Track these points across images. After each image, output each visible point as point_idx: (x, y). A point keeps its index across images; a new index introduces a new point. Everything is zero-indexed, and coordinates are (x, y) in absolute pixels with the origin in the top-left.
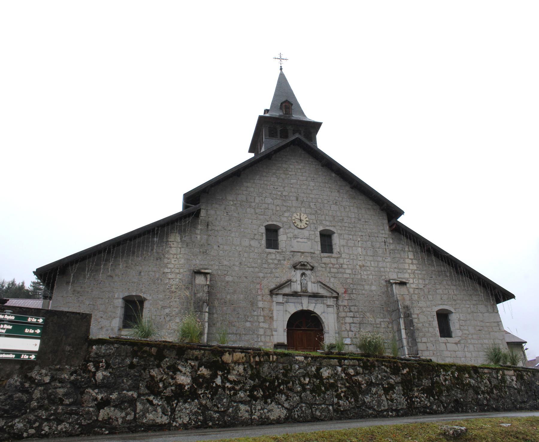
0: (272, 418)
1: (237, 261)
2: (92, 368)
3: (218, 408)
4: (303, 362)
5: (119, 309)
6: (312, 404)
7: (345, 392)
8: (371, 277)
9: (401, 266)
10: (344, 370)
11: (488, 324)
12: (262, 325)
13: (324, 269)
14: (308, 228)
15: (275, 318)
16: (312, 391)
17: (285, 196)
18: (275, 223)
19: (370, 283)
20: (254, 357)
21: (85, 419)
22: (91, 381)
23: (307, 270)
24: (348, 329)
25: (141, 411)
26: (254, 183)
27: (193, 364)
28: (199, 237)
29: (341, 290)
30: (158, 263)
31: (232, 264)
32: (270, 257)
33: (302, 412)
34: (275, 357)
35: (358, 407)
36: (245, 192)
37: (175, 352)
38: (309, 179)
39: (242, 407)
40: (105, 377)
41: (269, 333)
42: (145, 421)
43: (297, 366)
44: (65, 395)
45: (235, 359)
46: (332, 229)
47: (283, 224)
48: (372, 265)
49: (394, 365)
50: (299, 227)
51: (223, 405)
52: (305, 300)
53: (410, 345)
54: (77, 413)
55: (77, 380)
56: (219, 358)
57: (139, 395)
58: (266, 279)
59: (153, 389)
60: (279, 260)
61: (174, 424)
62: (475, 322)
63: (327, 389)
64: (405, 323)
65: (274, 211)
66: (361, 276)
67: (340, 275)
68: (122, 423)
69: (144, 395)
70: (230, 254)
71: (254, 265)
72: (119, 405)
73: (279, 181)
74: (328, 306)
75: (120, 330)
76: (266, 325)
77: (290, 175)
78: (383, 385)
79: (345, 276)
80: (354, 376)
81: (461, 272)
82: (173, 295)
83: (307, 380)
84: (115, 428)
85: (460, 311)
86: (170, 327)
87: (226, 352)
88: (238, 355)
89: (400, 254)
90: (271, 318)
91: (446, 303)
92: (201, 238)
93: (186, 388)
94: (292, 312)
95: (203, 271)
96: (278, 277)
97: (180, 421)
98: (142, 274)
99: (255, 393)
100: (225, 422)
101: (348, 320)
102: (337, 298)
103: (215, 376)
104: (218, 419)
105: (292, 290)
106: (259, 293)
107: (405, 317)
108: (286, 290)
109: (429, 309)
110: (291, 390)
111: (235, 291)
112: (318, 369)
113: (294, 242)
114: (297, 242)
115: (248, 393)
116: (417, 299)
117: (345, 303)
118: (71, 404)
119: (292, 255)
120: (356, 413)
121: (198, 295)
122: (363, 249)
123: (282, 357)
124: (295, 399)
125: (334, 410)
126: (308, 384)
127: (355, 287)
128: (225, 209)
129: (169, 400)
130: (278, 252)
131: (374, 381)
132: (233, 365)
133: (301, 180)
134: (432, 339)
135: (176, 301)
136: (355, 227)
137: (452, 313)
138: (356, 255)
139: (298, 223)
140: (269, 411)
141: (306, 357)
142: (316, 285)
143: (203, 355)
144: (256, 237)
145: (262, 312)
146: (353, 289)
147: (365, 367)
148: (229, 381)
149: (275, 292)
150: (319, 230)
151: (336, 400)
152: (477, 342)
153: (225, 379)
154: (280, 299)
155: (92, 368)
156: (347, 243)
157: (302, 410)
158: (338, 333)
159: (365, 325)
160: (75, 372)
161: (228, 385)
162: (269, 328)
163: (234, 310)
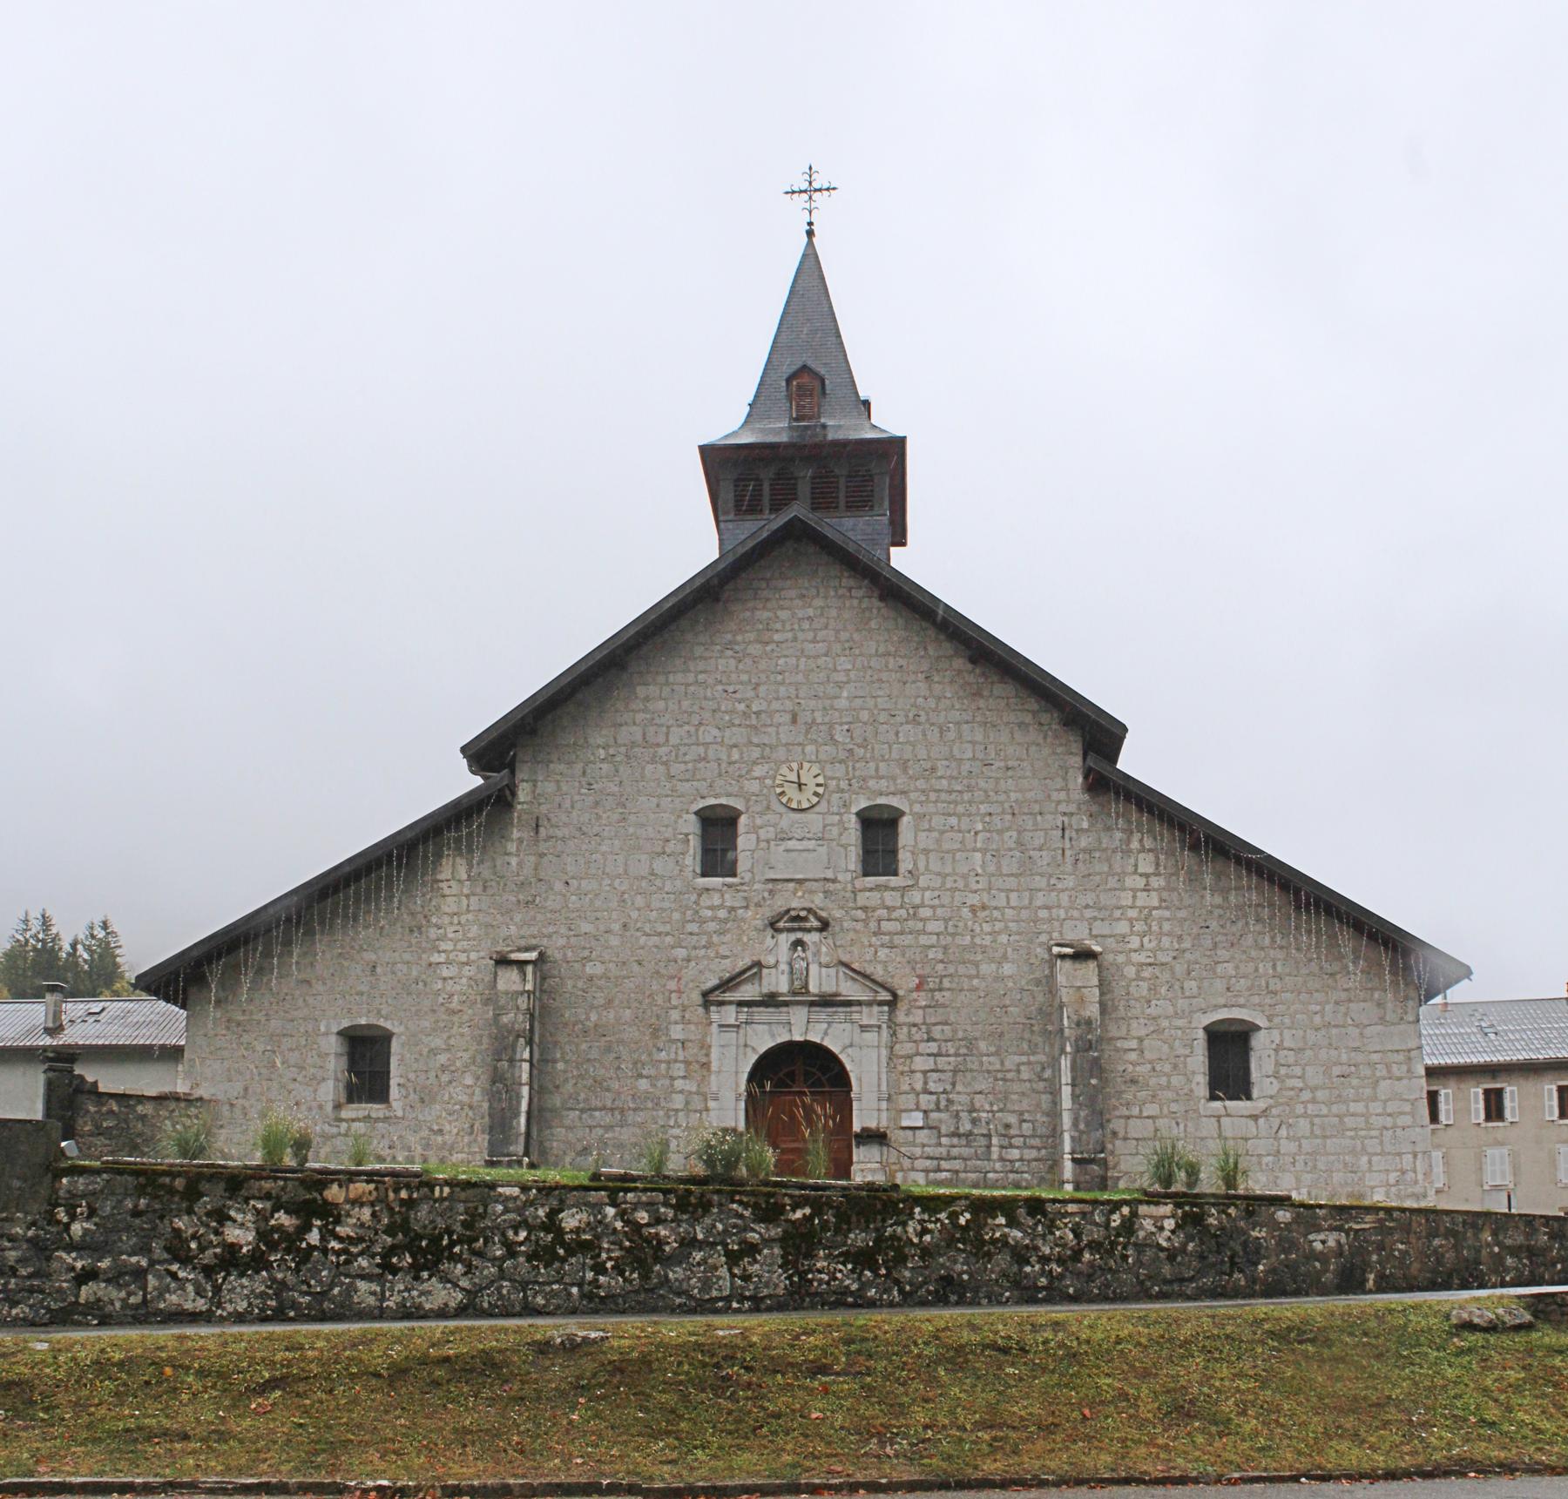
0: (427, 1306)
1: (615, 921)
2: (62, 1216)
3: (309, 1286)
4: (516, 1198)
5: (332, 1058)
6: (528, 1283)
7: (616, 1259)
8: (1003, 938)
9: (1106, 899)
10: (622, 1214)
11: (1375, 1057)
12: (679, 1084)
13: (859, 926)
14: (823, 807)
15: (714, 1066)
16: (530, 1257)
17: (758, 713)
18: (723, 801)
19: (998, 955)
20: (397, 1191)
21: (55, 1300)
22: (63, 1239)
23: (809, 930)
24: (919, 1086)
25: (155, 1289)
26: (667, 683)
27: (260, 1206)
28: (514, 861)
29: (904, 983)
30: (414, 941)
31: (602, 928)
32: (705, 901)
33: (501, 1297)
34: (447, 1190)
35: (647, 1291)
36: (640, 717)
37: (222, 1185)
38: (837, 648)
39: (362, 1285)
40: (86, 1231)
41: (697, 1103)
42: (162, 1306)
43: (500, 1208)
44: (18, 1261)
45: (352, 1196)
46: (894, 801)
47: (748, 801)
48: (1013, 904)
49: (767, 1202)
50: (794, 805)
51: (320, 1282)
52: (799, 1015)
53: (1082, 1126)
54: (42, 1292)
55: (37, 1236)
56: (316, 1195)
57: (152, 1263)
58: (693, 964)
59: (178, 1251)
60: (732, 909)
61: (219, 1312)
62: (1333, 1053)
63: (571, 1252)
64: (1073, 1069)
65: (724, 765)
66: (973, 937)
67: (908, 940)
68: (122, 1308)
69: (160, 1262)
70: (598, 903)
71: (661, 929)
72: (114, 1279)
73: (741, 666)
74: (864, 1028)
75: (338, 1107)
76: (691, 1086)
77: (778, 643)
78: (725, 1245)
79: (923, 940)
80: (648, 1225)
81: (1308, 904)
82: (455, 1019)
83: (523, 1235)
84: (110, 1316)
85: (1287, 1021)
86: (451, 1098)
87: (333, 1181)
88: (360, 1188)
89: (1108, 860)
90: (706, 1066)
91: (1242, 1001)
92: (520, 864)
93: (244, 1250)
94: (762, 1050)
95: (514, 956)
96: (726, 957)
97: (230, 1308)
98: (379, 970)
99: (394, 1260)
100: (323, 1311)
101: (920, 1063)
102: (893, 1003)
103: (307, 1228)
104: (309, 1307)
105: (765, 991)
106: (674, 1002)
107: (1077, 1050)
108: (748, 992)
109: (1180, 1023)
110: (479, 1254)
111: (610, 1001)
112: (553, 1214)
113: (778, 850)
114: (787, 851)
115: (378, 1260)
116: (1145, 993)
117: (917, 1017)
118: (30, 1276)
119: (771, 892)
120: (639, 1303)
121: (505, 1019)
122: (989, 857)
123: (463, 1190)
124: (486, 1272)
125: (583, 1296)
126: (521, 1244)
127: (951, 970)
128: (584, 773)
129: (208, 1271)
130: (729, 886)
131: (700, 1236)
132: (348, 1207)
133: (808, 657)
134: (1174, 1107)
135: (462, 1035)
136: (969, 789)
137: (1258, 1028)
138: (965, 877)
139: (791, 791)
140: (422, 1294)
141: (525, 1188)
142: (832, 971)
143: (283, 1189)
144: (670, 847)
145: (680, 1052)
146: (942, 977)
147: (681, 1207)
148: (340, 1239)
149: (712, 998)
150: (854, 809)
151: (590, 1275)
152: (1325, 1111)
153: (328, 1233)
154: (730, 1015)
155: (62, 1216)
156: (938, 841)
157: (500, 1293)
158: (889, 1099)
159: (968, 1075)
160: (34, 1224)
161: (334, 1244)
162: (697, 1093)
163: (608, 1049)
